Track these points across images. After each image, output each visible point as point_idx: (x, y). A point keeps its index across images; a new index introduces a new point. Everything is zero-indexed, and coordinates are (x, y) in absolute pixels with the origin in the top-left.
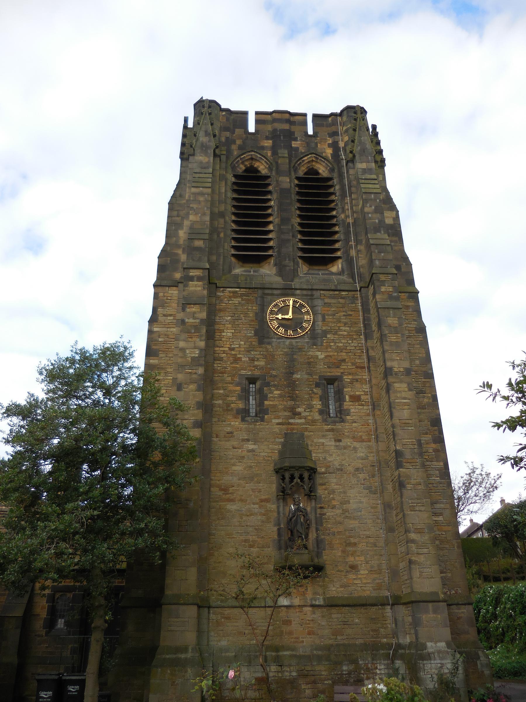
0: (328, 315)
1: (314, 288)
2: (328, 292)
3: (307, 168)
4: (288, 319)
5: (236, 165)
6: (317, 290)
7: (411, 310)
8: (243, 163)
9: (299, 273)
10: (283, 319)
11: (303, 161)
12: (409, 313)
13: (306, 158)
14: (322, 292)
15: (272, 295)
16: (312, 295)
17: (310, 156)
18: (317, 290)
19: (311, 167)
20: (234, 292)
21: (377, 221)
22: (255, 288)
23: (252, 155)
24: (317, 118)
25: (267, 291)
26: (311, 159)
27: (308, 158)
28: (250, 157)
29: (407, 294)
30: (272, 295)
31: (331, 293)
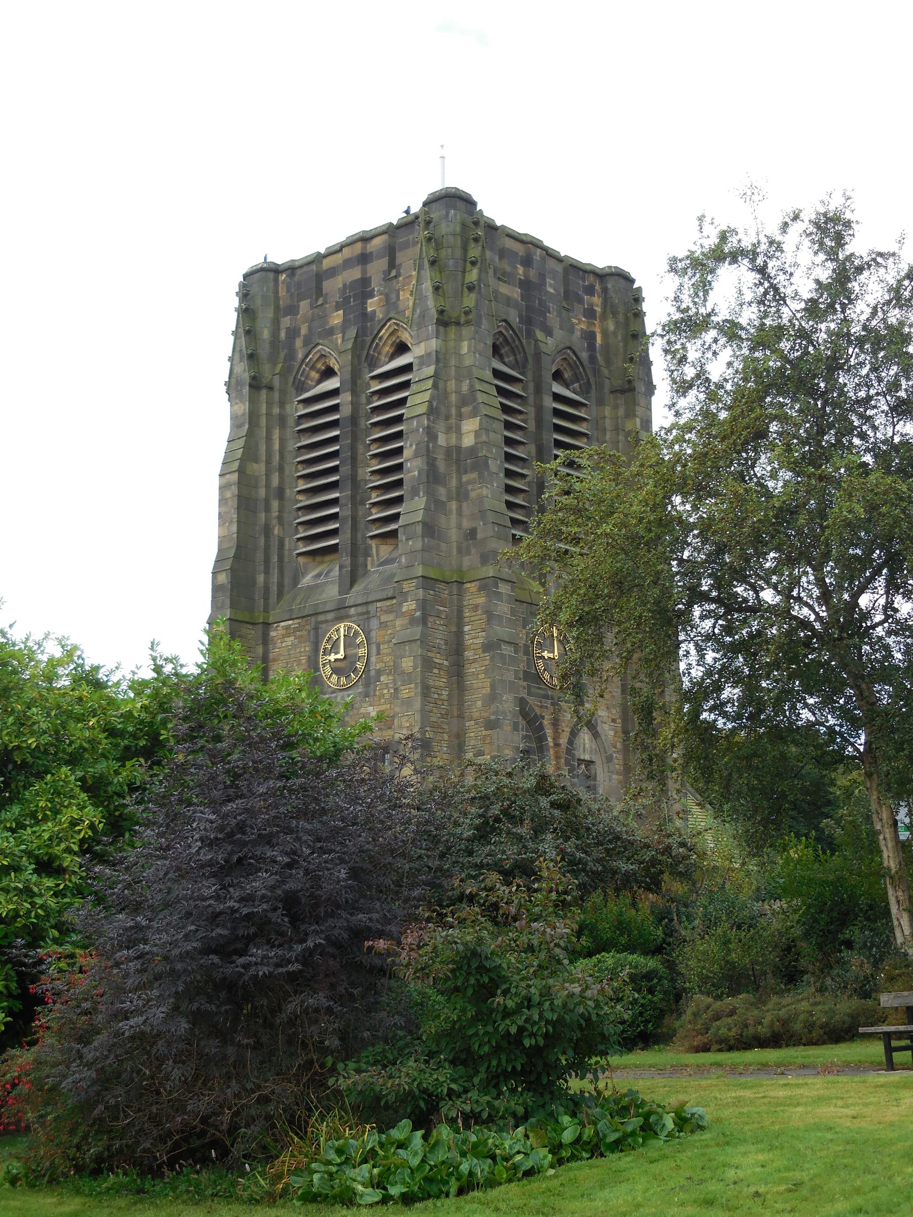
0: (384, 643)
1: (369, 600)
2: (385, 602)
3: (392, 345)
4: (340, 660)
5: (303, 379)
6: (373, 602)
7: (479, 612)
8: (313, 368)
9: (369, 567)
10: (336, 660)
11: (381, 338)
12: (477, 618)
13: (383, 331)
14: (379, 604)
15: (326, 621)
16: (368, 612)
17: (388, 324)
18: (373, 602)
19: (398, 341)
20: (287, 628)
21: (416, 473)
22: (308, 616)
23: (319, 351)
24: (402, 229)
25: (321, 618)
26: (391, 330)
27: (386, 331)
28: (318, 355)
29: (478, 583)
30: (326, 621)
31: (389, 603)
